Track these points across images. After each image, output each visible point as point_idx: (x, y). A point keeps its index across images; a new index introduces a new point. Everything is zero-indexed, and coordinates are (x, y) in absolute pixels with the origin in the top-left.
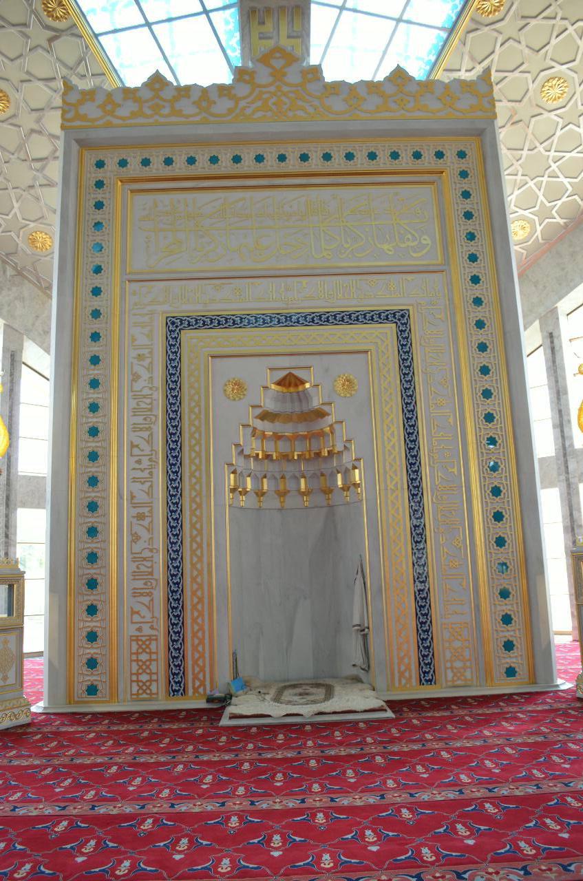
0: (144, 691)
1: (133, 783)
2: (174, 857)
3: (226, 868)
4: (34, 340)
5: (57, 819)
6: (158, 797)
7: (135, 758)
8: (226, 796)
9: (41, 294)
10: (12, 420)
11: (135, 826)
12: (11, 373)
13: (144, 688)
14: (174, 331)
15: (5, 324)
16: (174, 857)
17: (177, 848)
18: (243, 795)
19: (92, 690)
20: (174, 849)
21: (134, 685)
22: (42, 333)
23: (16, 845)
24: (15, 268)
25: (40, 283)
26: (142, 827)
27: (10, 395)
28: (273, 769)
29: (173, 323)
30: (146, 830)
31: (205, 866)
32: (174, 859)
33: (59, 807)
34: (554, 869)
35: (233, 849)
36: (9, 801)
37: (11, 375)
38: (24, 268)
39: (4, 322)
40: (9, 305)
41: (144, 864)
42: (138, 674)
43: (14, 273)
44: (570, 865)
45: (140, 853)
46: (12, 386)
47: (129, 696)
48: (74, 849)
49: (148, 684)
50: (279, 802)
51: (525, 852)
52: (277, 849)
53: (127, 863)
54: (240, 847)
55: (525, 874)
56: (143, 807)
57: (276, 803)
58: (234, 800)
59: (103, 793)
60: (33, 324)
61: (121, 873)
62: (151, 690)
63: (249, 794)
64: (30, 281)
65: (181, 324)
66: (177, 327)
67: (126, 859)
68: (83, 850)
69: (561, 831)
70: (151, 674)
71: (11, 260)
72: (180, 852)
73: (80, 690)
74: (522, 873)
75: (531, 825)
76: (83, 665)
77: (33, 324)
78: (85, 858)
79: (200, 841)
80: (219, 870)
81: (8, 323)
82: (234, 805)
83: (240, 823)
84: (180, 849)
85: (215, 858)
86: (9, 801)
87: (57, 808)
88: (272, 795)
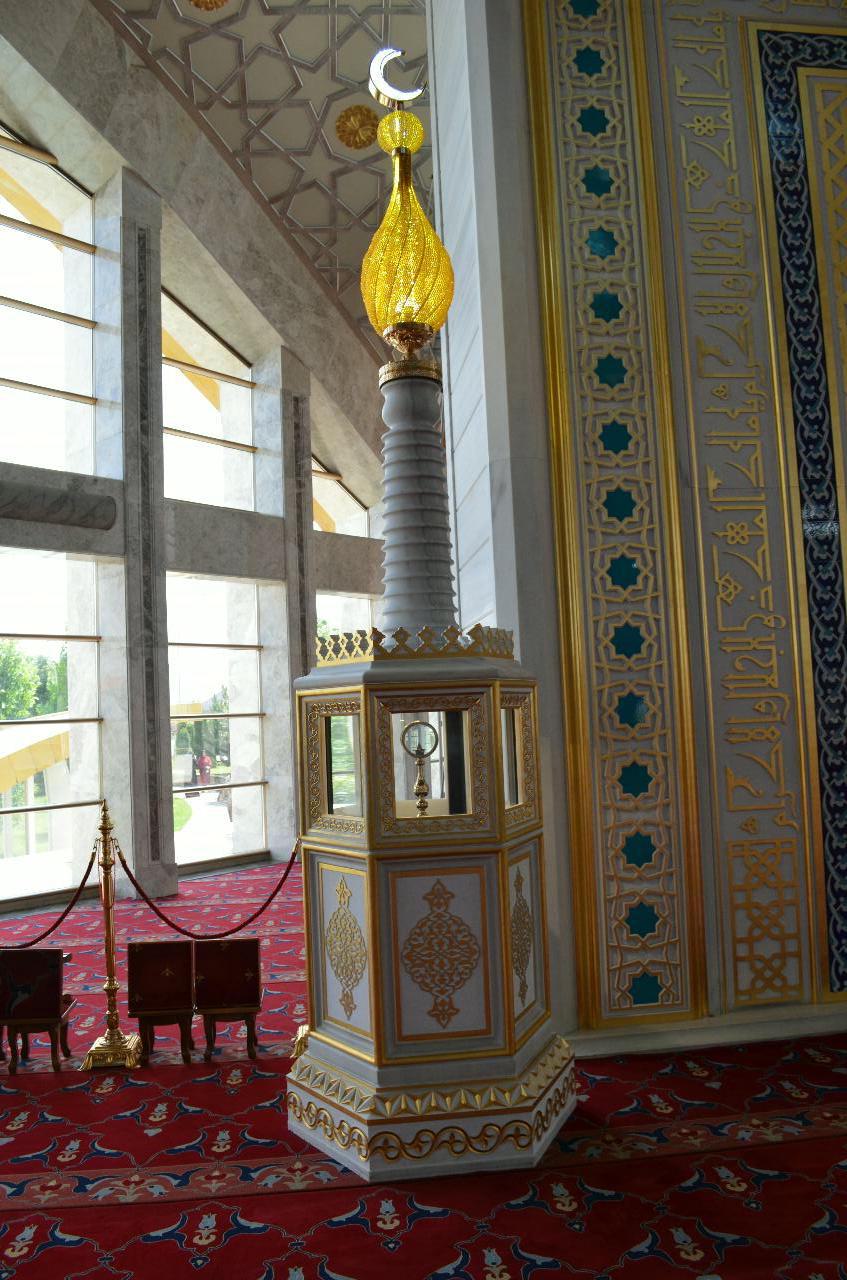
0: (769, 984)
1: (82, 1025)
2: (145, 1132)
3: (224, 1147)
4: (179, 212)
7: (86, 988)
9: (187, 116)
10: (146, 378)
12: (141, 275)
13: (768, 974)
14: (781, 67)
15: (124, 168)
16: (145, 1132)
19: (645, 988)
21: (743, 967)
22: (193, 200)
24: (141, 50)
25: (189, 90)
26: (98, 1090)
27: (141, 323)
28: (289, 998)
29: (776, 48)
31: (191, 1144)
32: (146, 1135)
33: (175, 1177)
34: (699, 1132)
35: (235, 1117)
37: (141, 280)
38: (162, 52)
39: (124, 162)
40: (132, 127)
41: (100, 1144)
42: (750, 941)
43: (138, 61)
44: (722, 1127)
45: (95, 1129)
46: (144, 303)
47: (731, 1000)
49: (776, 963)
51: (658, 1110)
53: (75, 1145)
54: (245, 1112)
55: (659, 1140)
59: (38, 1041)
60: (178, 178)
61: (67, 1159)
62: (784, 979)
64: (169, 85)
65: (797, 51)
66: (786, 57)
67: (74, 1138)
69: (708, 1079)
70: (782, 939)
71: (137, 28)
72: (154, 1125)
73: (612, 987)
74: (654, 1139)
75: (667, 1070)
76: (620, 927)
77: (178, 178)
78: (12, 1139)
79: (185, 1107)
80: (215, 1149)
81: (130, 166)
83: (244, 1079)
84: (155, 1120)
85: (208, 1130)
87: (175, 1182)
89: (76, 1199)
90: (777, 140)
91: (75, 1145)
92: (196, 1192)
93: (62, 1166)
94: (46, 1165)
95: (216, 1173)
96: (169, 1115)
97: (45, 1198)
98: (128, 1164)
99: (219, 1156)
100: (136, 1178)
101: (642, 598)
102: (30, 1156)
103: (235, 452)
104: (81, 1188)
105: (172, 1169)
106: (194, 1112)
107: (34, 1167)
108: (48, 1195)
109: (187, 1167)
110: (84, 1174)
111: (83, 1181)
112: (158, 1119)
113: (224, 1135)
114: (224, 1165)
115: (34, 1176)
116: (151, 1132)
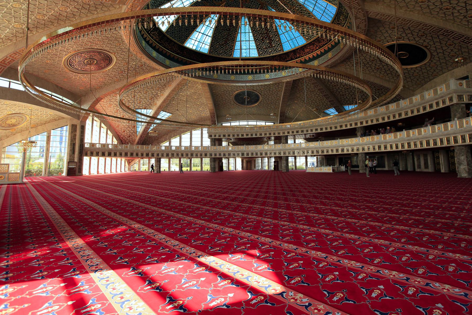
5: (373, 237)
6: (367, 275)
8: (424, 290)
11: (346, 298)
17: (380, 292)
18: (411, 287)
20: (382, 292)
23: (321, 277)
26: (342, 295)
30: (341, 293)
33: (430, 286)
36: (327, 262)
48: (385, 294)
50: (444, 289)
52: (439, 308)
54: (398, 298)
56: (427, 284)
57: (447, 289)
58: (418, 285)
63: (406, 286)
68: (333, 277)
72: (379, 289)
82: (418, 281)
86: (327, 262)
87: (381, 272)
88: (450, 297)
89: (329, 256)
90: (364, 135)
91: (360, 277)
92: (376, 268)
93: (365, 273)
94: (420, 289)
95: (416, 282)
96: (372, 291)
97: (335, 258)
98: (393, 280)
99: (414, 287)
100: (391, 276)
101: (36, 193)
102: (426, 294)
103: (193, 136)
104: (363, 267)
105: (340, 264)
106: (420, 308)
107: (333, 264)
108: (334, 258)
109: (376, 274)
110: (361, 269)
111: (361, 268)
112: (378, 291)
113: (410, 292)
114: (414, 284)
115: (373, 273)
116: (382, 287)
